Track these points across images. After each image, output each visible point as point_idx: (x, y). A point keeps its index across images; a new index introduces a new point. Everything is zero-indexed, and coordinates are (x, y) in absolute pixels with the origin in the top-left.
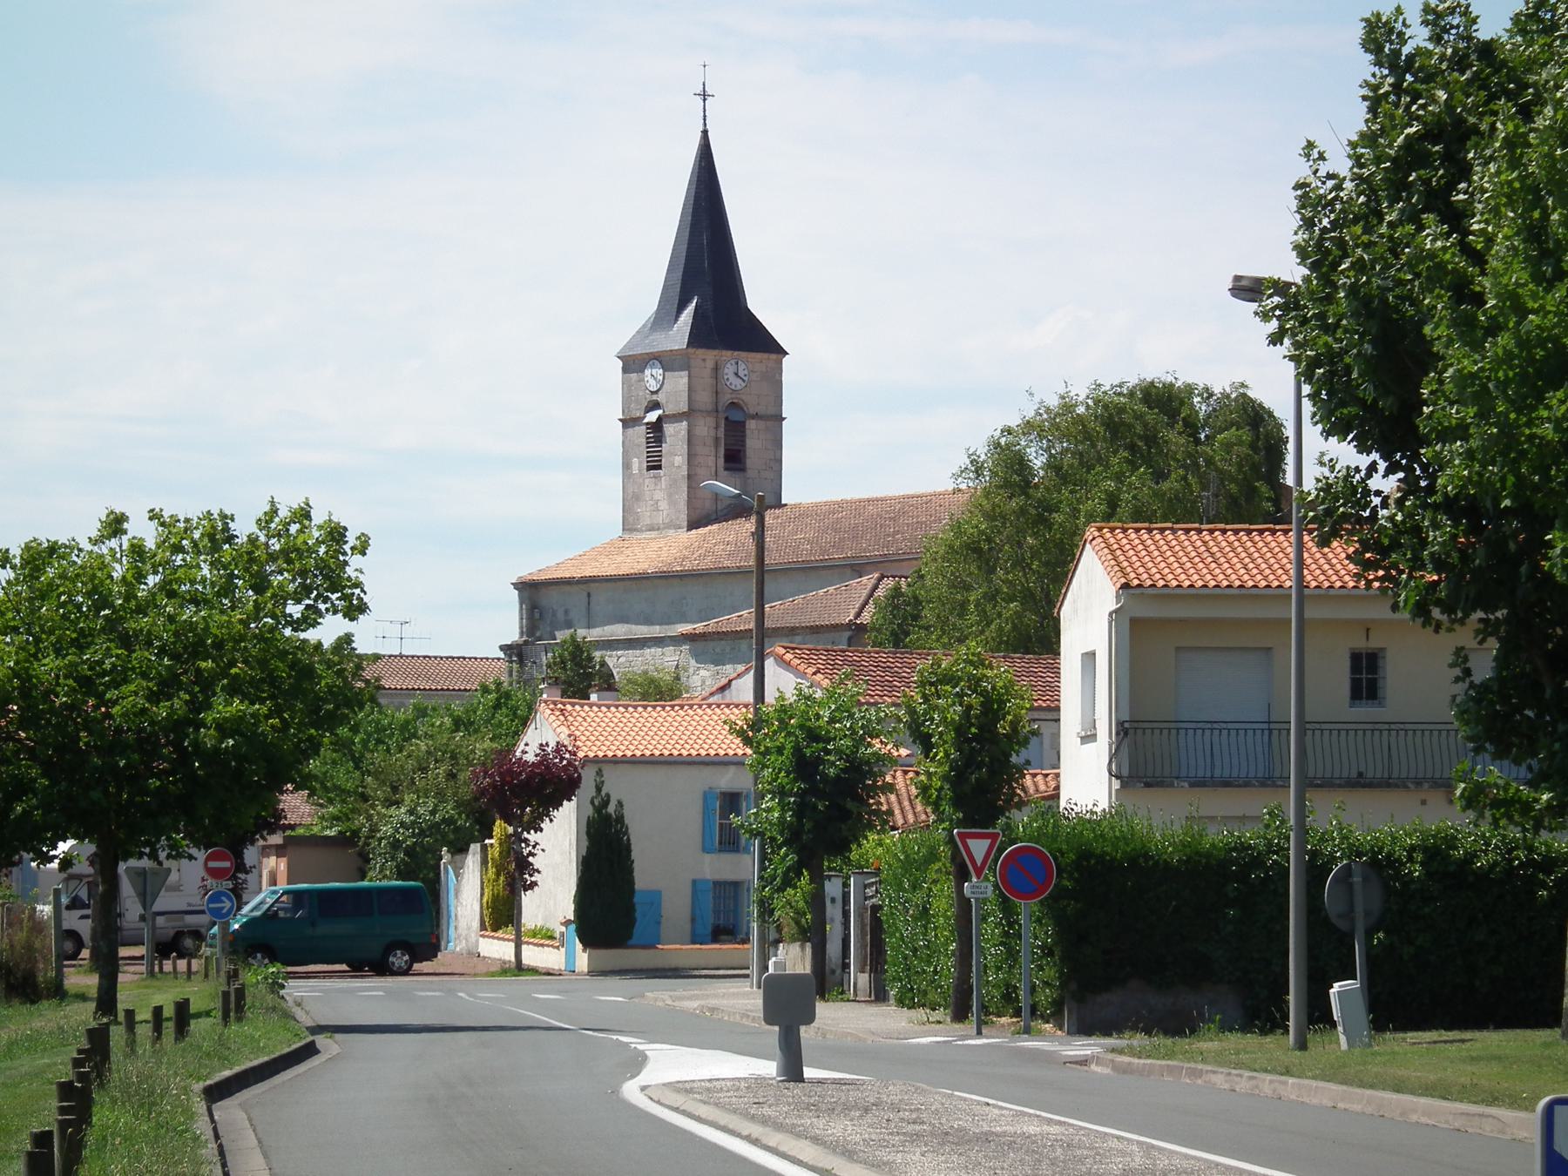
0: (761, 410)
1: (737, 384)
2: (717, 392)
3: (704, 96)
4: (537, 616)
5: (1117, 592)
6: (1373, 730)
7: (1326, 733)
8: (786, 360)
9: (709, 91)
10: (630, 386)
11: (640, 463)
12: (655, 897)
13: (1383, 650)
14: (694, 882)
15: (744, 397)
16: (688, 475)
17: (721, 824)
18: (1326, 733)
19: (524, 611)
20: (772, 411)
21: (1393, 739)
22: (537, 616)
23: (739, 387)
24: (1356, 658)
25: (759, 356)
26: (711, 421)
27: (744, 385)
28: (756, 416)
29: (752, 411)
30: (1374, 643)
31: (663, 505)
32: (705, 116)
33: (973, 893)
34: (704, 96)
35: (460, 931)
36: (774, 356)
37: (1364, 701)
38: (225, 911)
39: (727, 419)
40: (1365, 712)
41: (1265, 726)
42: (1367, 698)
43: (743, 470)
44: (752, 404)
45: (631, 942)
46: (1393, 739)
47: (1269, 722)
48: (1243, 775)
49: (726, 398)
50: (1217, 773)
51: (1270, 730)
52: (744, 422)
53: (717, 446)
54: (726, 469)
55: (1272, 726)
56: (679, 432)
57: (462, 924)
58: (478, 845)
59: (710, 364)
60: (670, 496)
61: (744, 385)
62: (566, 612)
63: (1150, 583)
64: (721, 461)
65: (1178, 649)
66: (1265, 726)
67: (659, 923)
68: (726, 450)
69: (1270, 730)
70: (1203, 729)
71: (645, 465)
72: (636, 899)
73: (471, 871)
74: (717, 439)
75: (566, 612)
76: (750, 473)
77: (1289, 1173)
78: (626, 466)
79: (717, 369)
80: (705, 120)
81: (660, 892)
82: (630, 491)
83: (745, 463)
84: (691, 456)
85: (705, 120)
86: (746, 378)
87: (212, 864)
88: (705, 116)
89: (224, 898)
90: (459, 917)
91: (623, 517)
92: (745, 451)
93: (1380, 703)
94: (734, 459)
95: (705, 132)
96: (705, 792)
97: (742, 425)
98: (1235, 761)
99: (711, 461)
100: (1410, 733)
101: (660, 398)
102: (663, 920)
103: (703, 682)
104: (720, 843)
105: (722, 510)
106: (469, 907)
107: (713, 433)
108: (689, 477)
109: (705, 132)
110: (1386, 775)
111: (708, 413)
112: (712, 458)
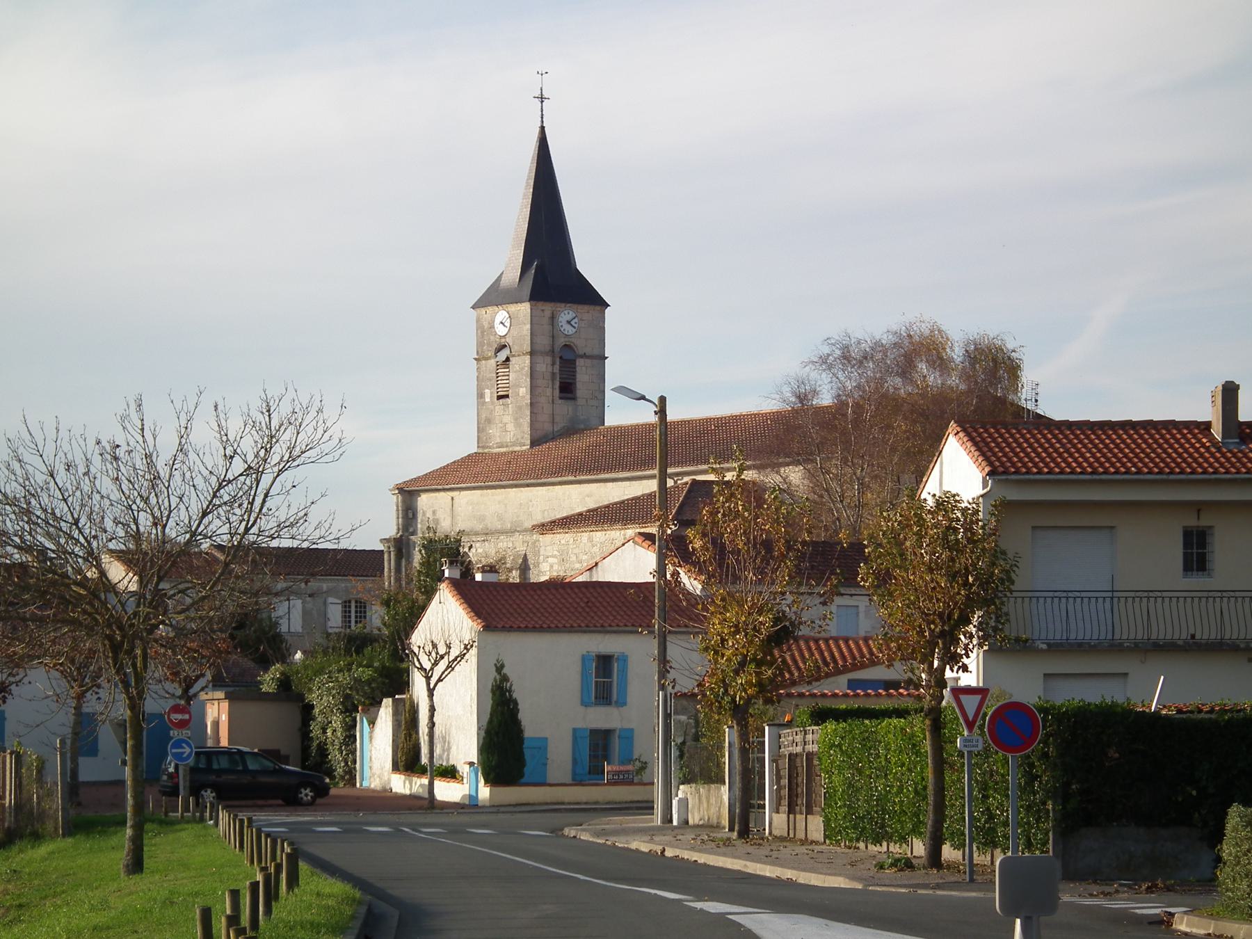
0: (588, 351)
1: (569, 330)
2: (553, 337)
3: (542, 99)
4: (410, 515)
5: (984, 479)
6: (1207, 598)
7: (1167, 600)
8: (608, 311)
9: (545, 95)
10: (482, 332)
11: (491, 393)
12: (542, 744)
13: (1211, 527)
14: (575, 730)
15: (573, 340)
16: (531, 403)
17: (596, 682)
18: (1167, 600)
19: (400, 512)
20: (596, 352)
21: (1225, 605)
22: (410, 515)
23: (570, 333)
24: (1187, 534)
25: (586, 307)
26: (549, 359)
27: (574, 330)
28: (584, 356)
29: (581, 352)
30: (1204, 522)
31: (510, 427)
32: (542, 115)
33: (965, 746)
34: (542, 99)
35: (374, 771)
36: (598, 308)
37: (1195, 573)
38: (185, 755)
39: (561, 358)
40: (1197, 582)
41: (1110, 594)
42: (1198, 570)
43: (574, 399)
44: (581, 345)
45: (523, 780)
46: (1225, 605)
47: (1113, 591)
48: (1095, 637)
49: (561, 341)
50: (1073, 636)
51: (1112, 598)
52: (575, 361)
53: (553, 380)
54: (561, 398)
55: (1116, 594)
56: (523, 368)
57: (376, 765)
58: (390, 699)
59: (548, 313)
60: (516, 419)
61: (574, 330)
62: (434, 512)
63: (1002, 469)
64: (557, 392)
65: (1034, 528)
66: (1110, 594)
67: (545, 765)
68: (560, 383)
69: (1112, 598)
70: (1060, 598)
71: (496, 395)
72: (526, 744)
73: (384, 718)
74: (553, 374)
75: (434, 512)
76: (580, 402)
77: (917, 936)
78: (481, 395)
79: (553, 318)
80: (542, 118)
81: (547, 739)
82: (483, 416)
83: (575, 394)
84: (533, 388)
85: (542, 118)
86: (576, 326)
87: (187, 717)
88: (542, 115)
89: (184, 745)
90: (373, 759)
91: (478, 437)
92: (575, 384)
93: (1209, 575)
94: (567, 389)
95: (543, 128)
96: (583, 655)
97: (573, 362)
98: (1088, 626)
99: (549, 392)
100: (1240, 600)
101: (509, 340)
102: (549, 762)
103: (551, 566)
104: (596, 698)
105: (557, 432)
106: (382, 750)
107: (550, 369)
108: (531, 404)
109: (543, 128)
110: (1146, 637)
111: (546, 354)
112: (550, 391)
